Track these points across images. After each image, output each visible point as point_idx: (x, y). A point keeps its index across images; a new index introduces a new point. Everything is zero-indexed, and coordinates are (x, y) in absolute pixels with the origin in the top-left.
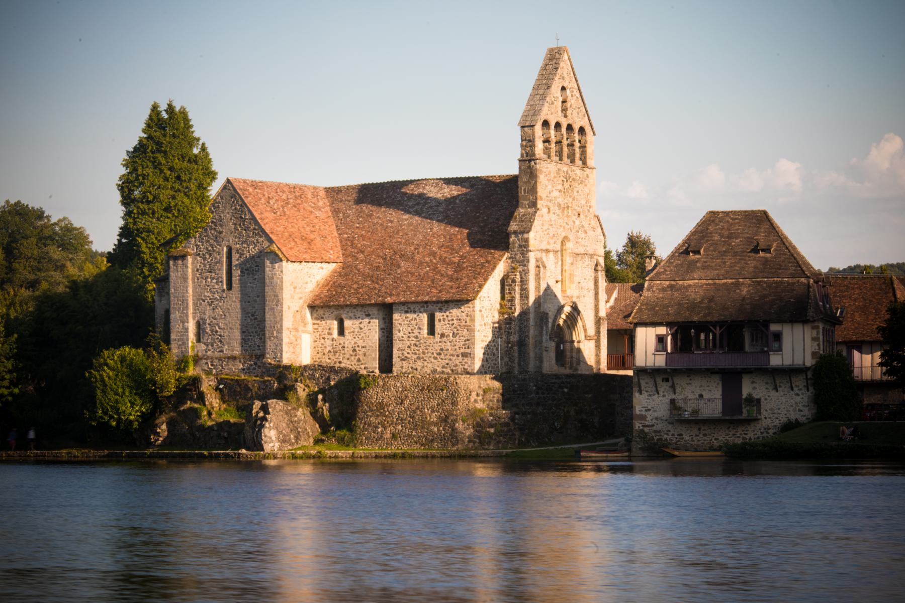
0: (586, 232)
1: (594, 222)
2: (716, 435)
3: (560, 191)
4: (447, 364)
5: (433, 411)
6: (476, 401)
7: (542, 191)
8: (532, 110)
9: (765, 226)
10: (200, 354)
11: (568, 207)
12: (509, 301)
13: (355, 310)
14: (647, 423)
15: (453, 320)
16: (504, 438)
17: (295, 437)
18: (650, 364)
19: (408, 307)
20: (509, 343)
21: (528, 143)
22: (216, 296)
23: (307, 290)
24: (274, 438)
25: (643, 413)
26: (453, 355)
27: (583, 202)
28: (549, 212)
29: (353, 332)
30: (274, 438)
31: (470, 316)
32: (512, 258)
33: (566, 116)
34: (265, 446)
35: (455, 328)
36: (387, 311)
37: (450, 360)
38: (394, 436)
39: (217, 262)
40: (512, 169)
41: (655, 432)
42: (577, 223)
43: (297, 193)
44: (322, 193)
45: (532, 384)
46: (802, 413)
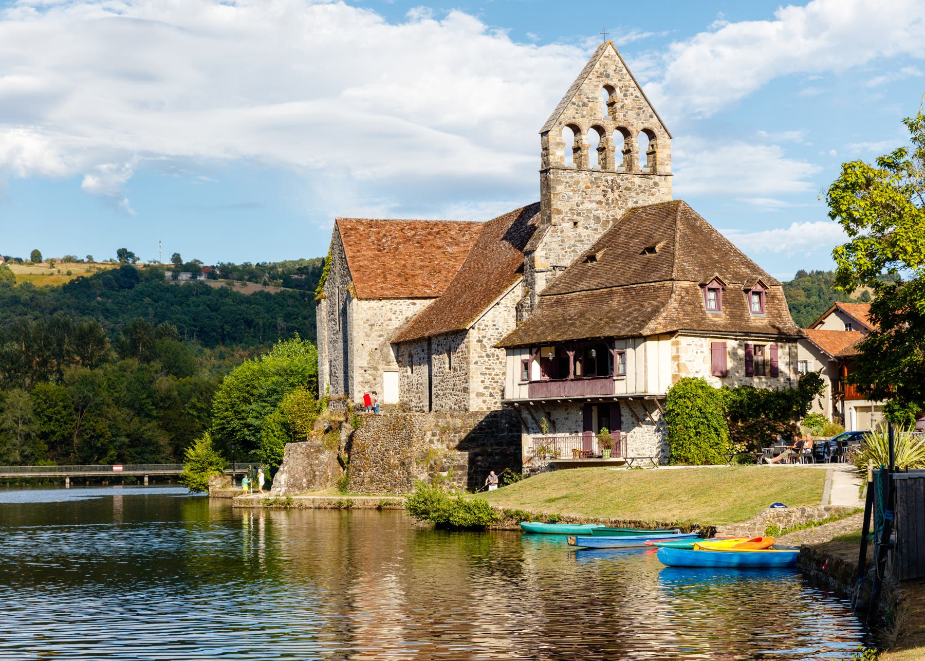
3: (600, 202)
6: (431, 441)
16: (458, 483)
17: (308, 481)
23: (390, 327)
24: (283, 483)
30: (283, 483)
33: (615, 119)
45: (504, 421)
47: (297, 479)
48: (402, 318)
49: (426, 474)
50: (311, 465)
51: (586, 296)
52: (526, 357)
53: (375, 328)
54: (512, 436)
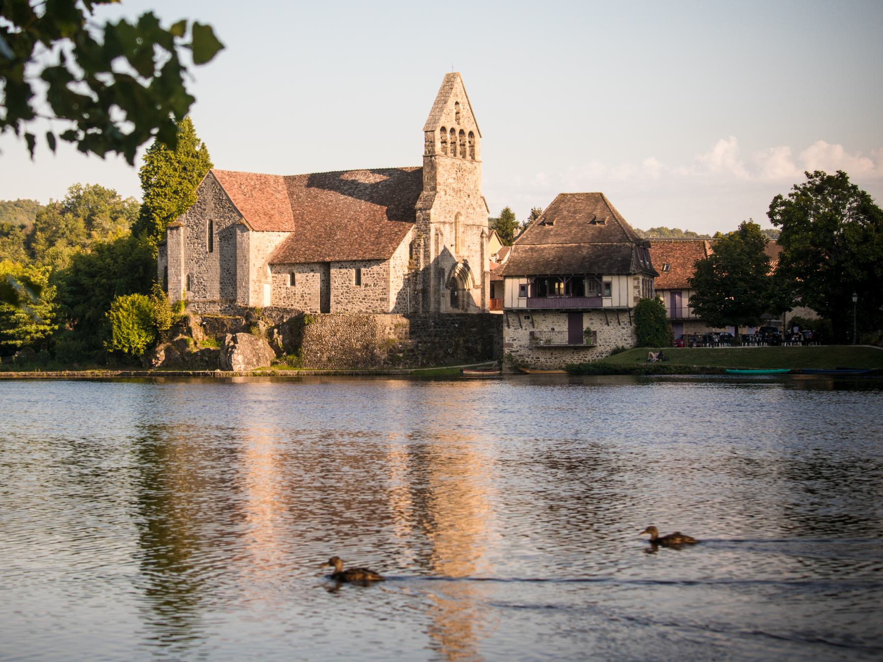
2: (564, 358)
3: (454, 179)
5: (358, 341)
6: (389, 333)
7: (440, 179)
8: (433, 119)
9: (601, 204)
12: (416, 260)
18: (515, 306)
20: (415, 291)
22: (201, 256)
24: (241, 361)
25: (511, 342)
26: (374, 300)
30: (241, 361)
34: (234, 367)
36: (326, 267)
40: (418, 162)
43: (263, 181)
52: (524, 281)
54: (437, 331)
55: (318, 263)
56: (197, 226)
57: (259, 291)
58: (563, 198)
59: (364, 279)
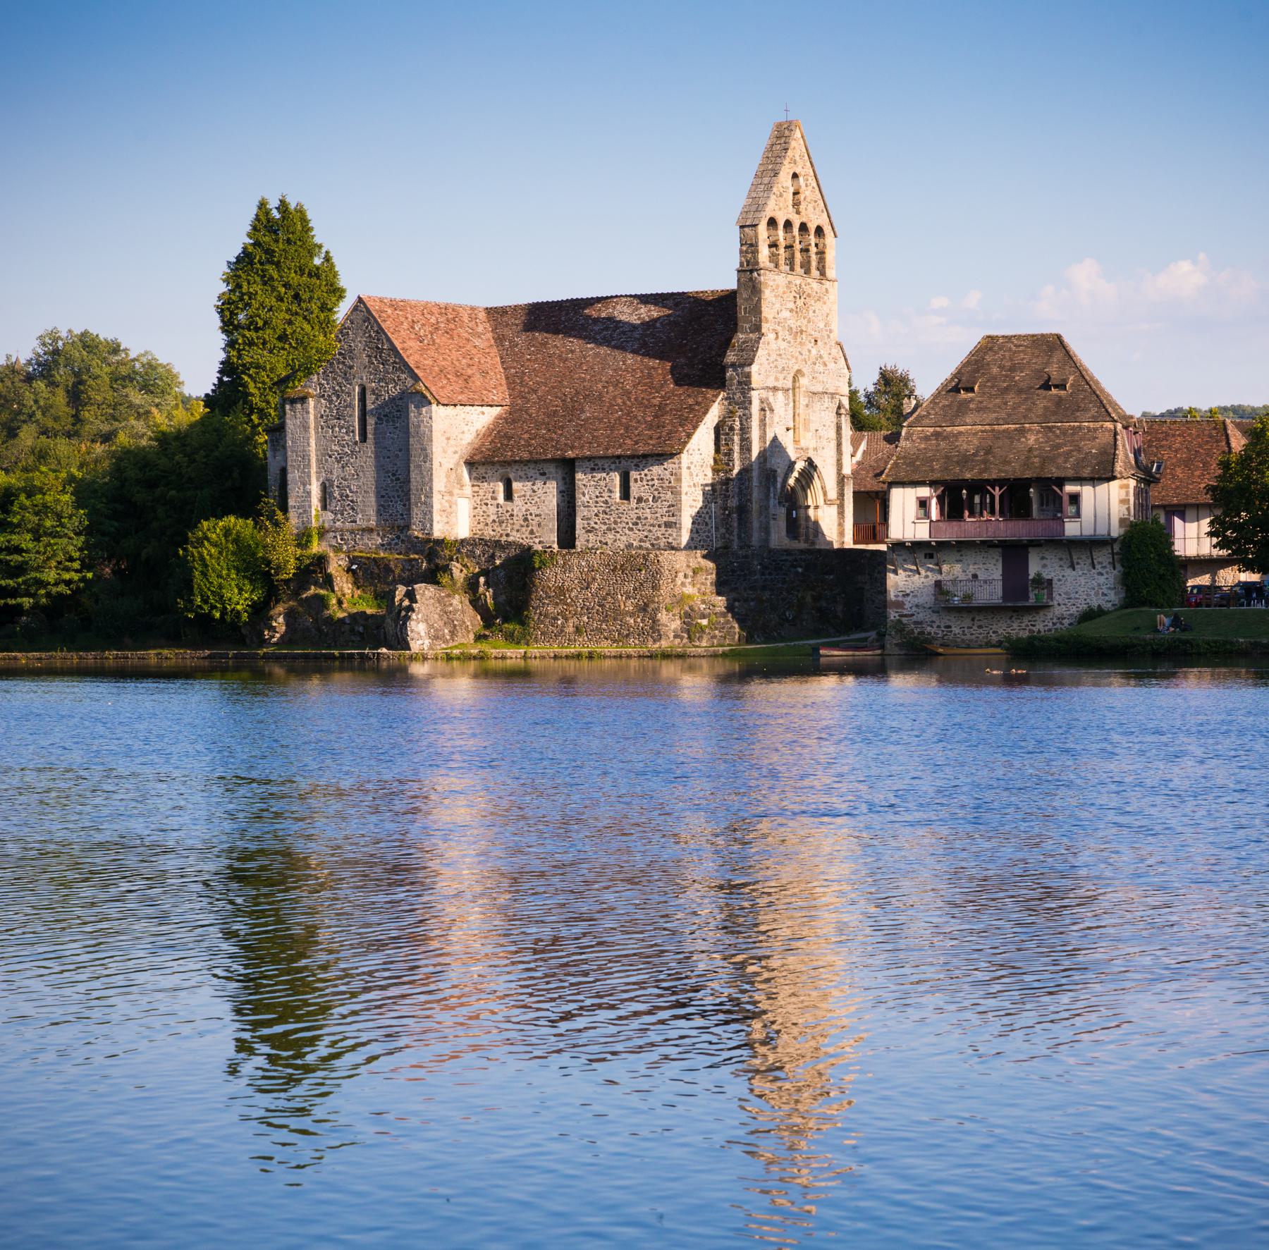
0: (825, 365)
1: (836, 351)
3: (791, 311)
4: (646, 537)
5: (628, 598)
6: (683, 584)
7: (767, 311)
8: (755, 205)
9: (1059, 355)
10: (326, 525)
11: (802, 332)
12: (725, 454)
13: (526, 468)
14: (905, 612)
15: (653, 480)
19: (596, 464)
20: (725, 509)
21: (749, 247)
22: (346, 450)
24: (423, 634)
25: (900, 599)
26: (653, 525)
27: (821, 325)
28: (777, 338)
29: (524, 496)
31: (676, 474)
32: (730, 398)
33: (798, 213)
35: (656, 490)
37: (650, 531)
38: (578, 630)
39: (347, 406)
40: (729, 282)
41: (916, 623)
42: (814, 352)
43: (450, 316)
44: (482, 315)
46: (1107, 598)
47: (437, 630)
48: (473, 430)
49: (678, 622)
50: (446, 613)
51: (982, 431)
52: (925, 492)
53: (452, 442)
55: (553, 460)
56: (338, 397)
57: (449, 512)
58: (990, 344)
59: (635, 490)
